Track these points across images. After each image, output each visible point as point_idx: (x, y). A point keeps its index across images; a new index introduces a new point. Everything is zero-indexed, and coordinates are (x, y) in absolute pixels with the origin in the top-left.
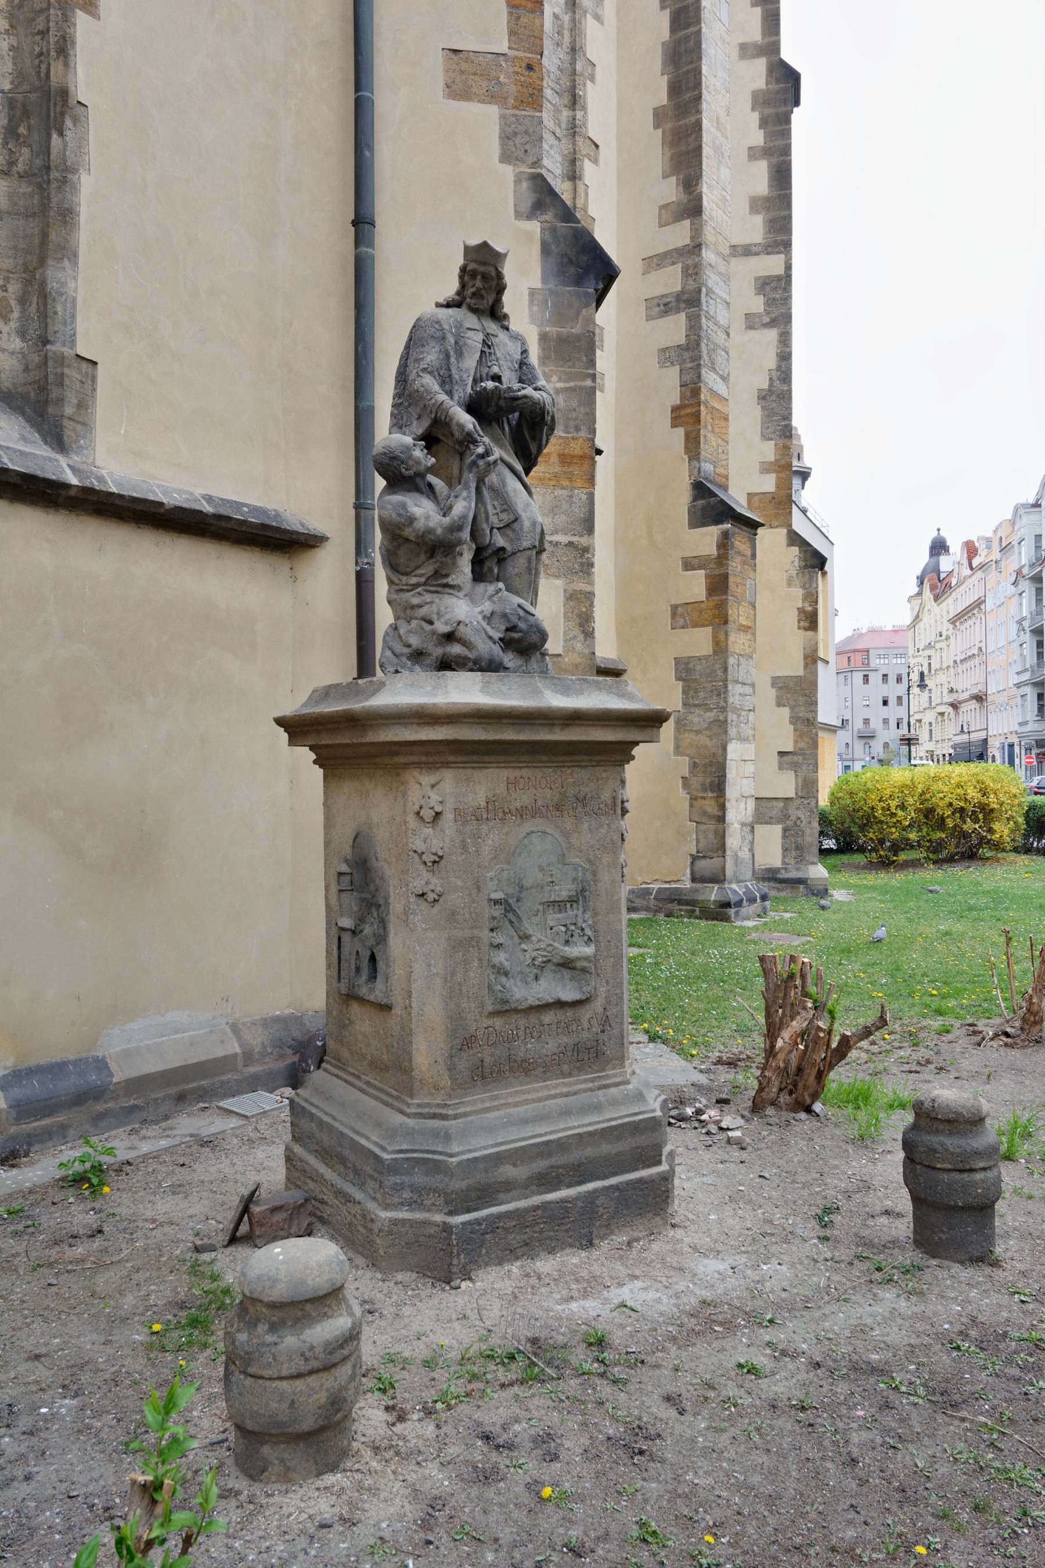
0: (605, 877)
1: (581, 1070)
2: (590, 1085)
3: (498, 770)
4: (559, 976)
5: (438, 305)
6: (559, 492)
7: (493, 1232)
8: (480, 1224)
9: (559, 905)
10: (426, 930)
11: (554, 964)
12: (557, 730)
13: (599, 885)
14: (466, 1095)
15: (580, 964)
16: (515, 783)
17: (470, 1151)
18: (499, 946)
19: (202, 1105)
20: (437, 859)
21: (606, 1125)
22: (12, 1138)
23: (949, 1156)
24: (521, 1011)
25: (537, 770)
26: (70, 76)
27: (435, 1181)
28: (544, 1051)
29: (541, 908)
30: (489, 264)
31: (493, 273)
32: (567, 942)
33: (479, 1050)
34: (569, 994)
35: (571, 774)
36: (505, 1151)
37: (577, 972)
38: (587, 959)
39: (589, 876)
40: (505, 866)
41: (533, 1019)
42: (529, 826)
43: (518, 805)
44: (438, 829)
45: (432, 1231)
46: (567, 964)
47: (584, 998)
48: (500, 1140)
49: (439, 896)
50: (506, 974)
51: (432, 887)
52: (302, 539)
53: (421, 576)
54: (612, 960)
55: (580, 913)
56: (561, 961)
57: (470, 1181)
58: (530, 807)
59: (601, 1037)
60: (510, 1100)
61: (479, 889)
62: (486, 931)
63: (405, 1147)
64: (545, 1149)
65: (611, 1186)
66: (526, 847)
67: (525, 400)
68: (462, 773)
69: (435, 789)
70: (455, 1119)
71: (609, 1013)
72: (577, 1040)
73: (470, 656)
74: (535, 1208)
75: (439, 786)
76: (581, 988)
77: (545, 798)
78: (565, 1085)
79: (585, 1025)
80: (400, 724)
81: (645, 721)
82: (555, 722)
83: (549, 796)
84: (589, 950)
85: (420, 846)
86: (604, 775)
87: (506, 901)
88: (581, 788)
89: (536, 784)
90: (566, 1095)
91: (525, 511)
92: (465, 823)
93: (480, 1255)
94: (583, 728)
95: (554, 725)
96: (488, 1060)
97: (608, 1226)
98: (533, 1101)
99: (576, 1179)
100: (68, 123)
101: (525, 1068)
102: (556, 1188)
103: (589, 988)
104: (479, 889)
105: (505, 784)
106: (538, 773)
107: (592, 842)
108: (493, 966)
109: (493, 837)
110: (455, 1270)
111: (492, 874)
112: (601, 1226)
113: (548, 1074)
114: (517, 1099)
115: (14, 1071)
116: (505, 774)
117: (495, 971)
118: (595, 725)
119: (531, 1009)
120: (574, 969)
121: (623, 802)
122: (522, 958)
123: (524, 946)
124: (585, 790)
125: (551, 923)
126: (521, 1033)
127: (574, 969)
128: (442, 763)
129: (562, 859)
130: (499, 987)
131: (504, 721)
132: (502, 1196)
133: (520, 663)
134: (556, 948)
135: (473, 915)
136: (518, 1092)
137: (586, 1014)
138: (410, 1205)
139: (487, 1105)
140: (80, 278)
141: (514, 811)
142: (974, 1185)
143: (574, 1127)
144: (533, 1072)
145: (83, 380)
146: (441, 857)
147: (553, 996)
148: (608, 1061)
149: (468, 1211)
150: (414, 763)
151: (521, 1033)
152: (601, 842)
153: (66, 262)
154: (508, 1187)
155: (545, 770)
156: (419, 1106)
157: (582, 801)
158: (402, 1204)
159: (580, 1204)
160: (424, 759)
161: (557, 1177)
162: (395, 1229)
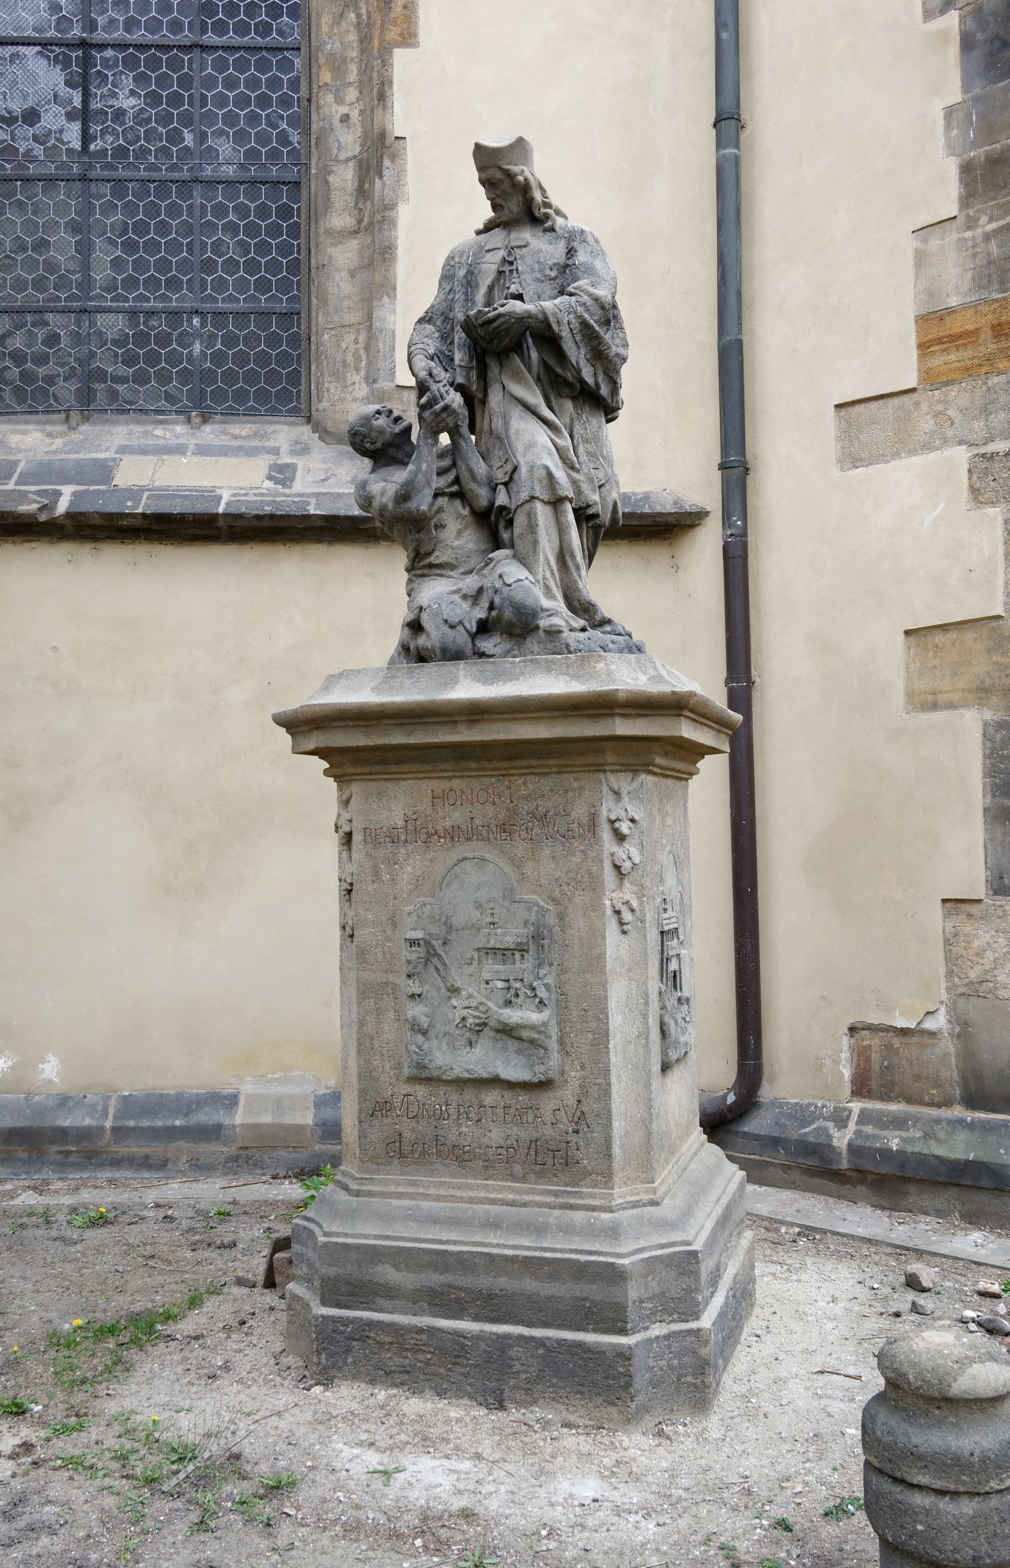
0: (578, 923)
1: (540, 1176)
3: (419, 782)
4: (500, 1045)
5: (479, 233)
6: (994, 380)
9: (503, 954)
11: (492, 1029)
12: (462, 727)
13: (569, 932)
14: (379, 1172)
15: (525, 1034)
16: (444, 797)
17: (346, 1235)
21: (537, 1254)
22: (317, 1155)
23: (875, 1444)
25: (474, 781)
26: (388, 116)
28: (485, 1140)
30: (489, 167)
31: (498, 175)
32: (508, 1003)
34: (514, 1070)
35: (525, 784)
36: (385, 1247)
38: (532, 1027)
40: (427, 900)
41: (469, 1095)
42: (462, 850)
43: (447, 824)
46: (507, 1031)
47: (535, 1080)
48: (390, 1233)
50: (424, 1033)
52: (671, 520)
54: (590, 1035)
56: (499, 1027)
57: (341, 1271)
58: (464, 827)
59: (572, 1138)
60: (432, 1191)
61: (394, 925)
62: (404, 977)
64: (440, 1260)
65: (532, 1339)
66: (456, 876)
67: (501, 320)
68: (373, 786)
70: (357, 1196)
71: (585, 1109)
72: (535, 1135)
74: (420, 1331)
77: (485, 816)
78: (513, 1190)
79: (548, 1117)
83: (491, 813)
86: (576, 785)
87: (428, 943)
88: (539, 802)
89: (471, 800)
90: (512, 1204)
91: (525, 455)
92: (377, 845)
94: (501, 724)
95: (455, 722)
96: (407, 1135)
100: (387, 162)
101: (460, 1157)
102: (457, 1314)
103: (543, 1068)
104: (394, 925)
105: (429, 799)
107: (558, 874)
109: (412, 864)
111: (411, 908)
113: (490, 1172)
115: (334, 1092)
116: (428, 786)
118: (515, 719)
119: (461, 1083)
120: (520, 1039)
122: (451, 1016)
123: (454, 1002)
124: (544, 805)
125: (486, 976)
127: (520, 1039)
129: (509, 895)
131: (384, 722)
132: (381, 1301)
133: (508, 647)
135: (388, 956)
136: (445, 1183)
137: (547, 1103)
139: (401, 1189)
140: (397, 311)
141: (441, 833)
142: (911, 1512)
144: (469, 1164)
145: (405, 408)
147: (490, 1070)
148: (586, 1174)
149: (338, 1306)
152: (572, 875)
153: (386, 298)
154: (389, 1293)
155: (484, 780)
157: (543, 819)
161: (458, 1301)
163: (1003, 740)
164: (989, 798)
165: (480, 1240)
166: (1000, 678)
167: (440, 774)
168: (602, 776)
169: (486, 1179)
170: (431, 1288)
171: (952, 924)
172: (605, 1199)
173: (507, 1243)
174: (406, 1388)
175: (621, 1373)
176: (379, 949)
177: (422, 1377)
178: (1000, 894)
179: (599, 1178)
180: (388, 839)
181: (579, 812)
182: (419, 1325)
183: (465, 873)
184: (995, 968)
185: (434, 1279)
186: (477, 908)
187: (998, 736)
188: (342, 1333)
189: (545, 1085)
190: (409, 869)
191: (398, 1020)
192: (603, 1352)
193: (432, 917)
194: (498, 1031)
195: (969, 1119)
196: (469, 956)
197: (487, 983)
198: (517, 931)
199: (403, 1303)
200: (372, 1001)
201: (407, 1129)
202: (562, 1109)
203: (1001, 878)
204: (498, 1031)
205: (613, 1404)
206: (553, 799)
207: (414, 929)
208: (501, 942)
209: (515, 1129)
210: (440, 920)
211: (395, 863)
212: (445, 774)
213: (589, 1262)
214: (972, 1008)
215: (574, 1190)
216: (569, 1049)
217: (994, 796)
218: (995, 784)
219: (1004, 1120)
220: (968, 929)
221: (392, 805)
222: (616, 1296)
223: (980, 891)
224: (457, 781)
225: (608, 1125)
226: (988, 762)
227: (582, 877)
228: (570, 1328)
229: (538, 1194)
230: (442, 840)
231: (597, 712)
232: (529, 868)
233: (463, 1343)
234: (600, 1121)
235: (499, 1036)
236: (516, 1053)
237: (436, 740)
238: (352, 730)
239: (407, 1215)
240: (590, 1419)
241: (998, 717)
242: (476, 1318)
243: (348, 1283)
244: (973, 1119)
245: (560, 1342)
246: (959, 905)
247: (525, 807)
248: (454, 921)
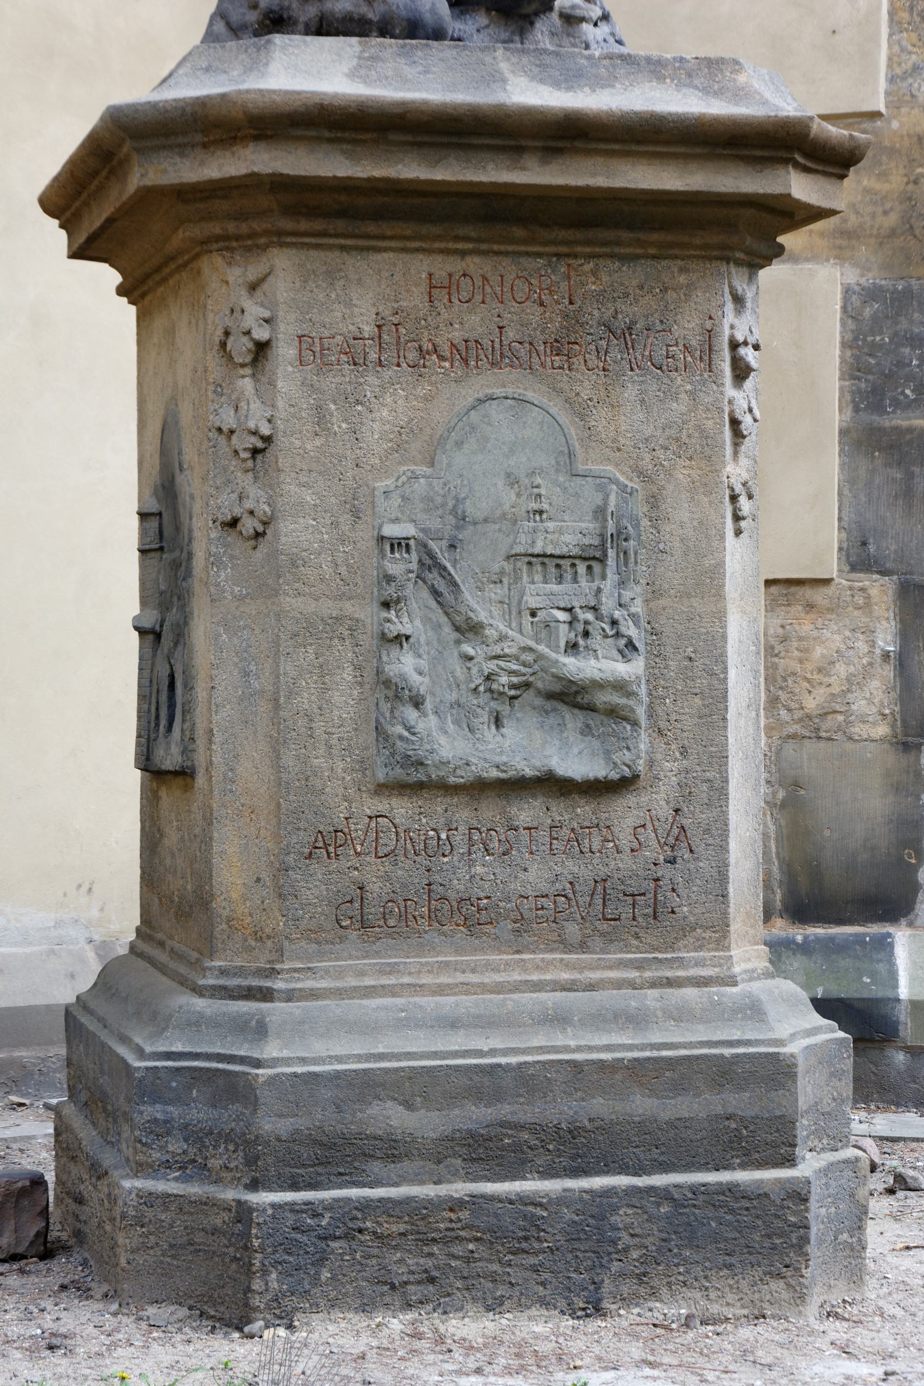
0: (681, 513)
1: (609, 939)
2: (633, 974)
3: (406, 257)
4: (552, 720)
7: (347, 1236)
8: (316, 1215)
9: (554, 563)
10: (241, 598)
11: (539, 692)
12: (531, 161)
13: (666, 528)
14: (321, 955)
17: (303, 1061)
18: (400, 639)
19: (15, 1099)
20: (260, 445)
21: (647, 1054)
24: (456, 789)
25: (506, 261)
27: (226, 1117)
28: (516, 886)
29: (508, 567)
32: (572, 648)
33: (355, 862)
34: (577, 761)
35: (594, 273)
36: (387, 1071)
37: (598, 718)
38: (620, 686)
39: (641, 509)
41: (490, 811)
42: (483, 382)
43: (457, 335)
44: (264, 379)
45: (219, 1222)
46: (570, 697)
47: (614, 775)
48: (381, 1049)
49: (265, 523)
51: (249, 504)
54: (697, 700)
55: (608, 585)
56: (557, 687)
57: (302, 1123)
58: (486, 343)
59: (665, 871)
60: (426, 979)
61: (356, 514)
63: (178, 1047)
64: (486, 1082)
65: (651, 1190)
66: (473, 428)
68: (318, 259)
69: (259, 293)
70: (289, 1000)
71: (686, 822)
72: (603, 871)
73: (371, 15)
74: (456, 1205)
75: (265, 286)
76: (607, 754)
78: (568, 966)
80: (170, 147)
81: (763, 147)
82: (523, 143)
83: (535, 320)
84: (631, 669)
85: (228, 419)
86: (682, 279)
89: (504, 295)
92: (325, 366)
93: (315, 1280)
94: (600, 160)
96: (375, 887)
97: (641, 1278)
98: (484, 988)
99: (565, 1161)
101: (472, 918)
103: (628, 756)
105: (424, 287)
106: (509, 269)
107: (649, 432)
108: (387, 683)
110: (256, 1301)
111: (389, 482)
112: (622, 1275)
113: (527, 938)
114: (444, 979)
117: (391, 693)
119: (481, 788)
120: (590, 708)
121: (734, 345)
123: (468, 649)
124: (628, 311)
125: (533, 602)
126: (459, 838)
127: (590, 708)
128: (267, 233)
130: (399, 730)
131: (392, 137)
132: (376, 1167)
134: (540, 657)
135: (343, 570)
136: (447, 964)
137: (625, 813)
138: (182, 1168)
139: (368, 981)
141: (446, 350)
143: (566, 1049)
144: (488, 928)
146: (268, 439)
149: (295, 1187)
150: (218, 238)
151: (459, 838)
152: (672, 432)
154: (393, 1150)
155: (526, 262)
156: (223, 972)
158: (167, 1165)
159: (568, 1214)
160: (231, 227)
161: (517, 1148)
162: (149, 1213)
163: (875, 318)
164: (849, 413)
165: (543, 1043)
166: (873, 216)
167: (451, 245)
168: (724, 268)
169: (518, 952)
170: (469, 1131)
171: (779, 622)
172: (721, 965)
173: (593, 1043)
174: (430, 1307)
175: (794, 1225)
176: (325, 559)
177: (459, 1284)
178: (861, 571)
179: (707, 935)
180: (344, 358)
181: (688, 326)
182: (456, 1195)
183: (489, 424)
184: (849, 690)
185: (475, 1115)
186: (512, 485)
187: (868, 312)
188: (311, 1229)
189: (623, 785)
190: (385, 413)
191: (361, 684)
192: (766, 1195)
193: (428, 499)
194: (551, 696)
195: (799, 939)
196: (496, 567)
197: (533, 614)
198: (583, 525)
199: (418, 1163)
200: (311, 650)
201: (375, 877)
202: (649, 826)
203: (864, 544)
204: (551, 696)
205: (780, 1276)
206: (643, 301)
207: (396, 520)
208: (555, 544)
209: (569, 863)
210: (443, 505)
211: (358, 402)
212: (460, 246)
213: (737, 1056)
214: (807, 758)
215: (669, 956)
216: (663, 724)
217: (856, 410)
218: (859, 391)
219: (856, 935)
220: (806, 628)
221: (354, 296)
222: (779, 1104)
223: (831, 566)
224: (477, 259)
225: (723, 848)
226: (849, 353)
227: (689, 436)
228: (705, 1167)
229: (610, 968)
230: (447, 364)
231: (766, 154)
232: (600, 419)
233: (533, 1215)
234: (711, 841)
235: (549, 705)
236: (582, 733)
237: (484, 179)
238: (325, 146)
239: (400, 1020)
240: (743, 1307)
241: (867, 281)
242: (548, 1173)
243: (316, 1142)
244: (806, 938)
245: (695, 1189)
246: (793, 589)
247: (596, 312)
248: (469, 508)
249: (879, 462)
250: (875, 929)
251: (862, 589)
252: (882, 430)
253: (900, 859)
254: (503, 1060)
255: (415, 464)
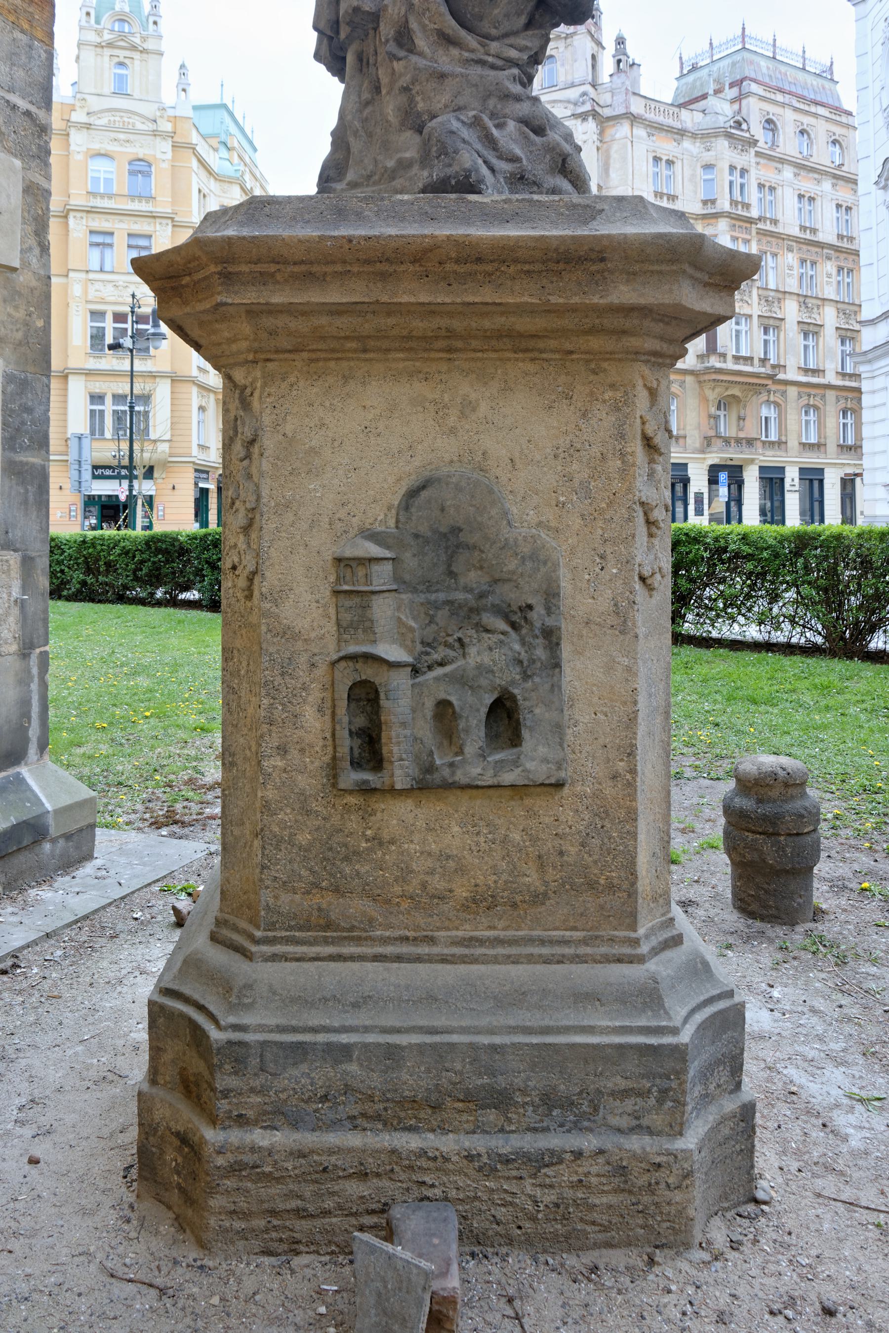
53: (521, 50)
166: (12, 330)
203: (7, 532)
249: (14, 482)
250: (11, 771)
251: (7, 561)
252: (15, 462)
253: (22, 725)
254: (455, 1038)
255: (455, 272)
